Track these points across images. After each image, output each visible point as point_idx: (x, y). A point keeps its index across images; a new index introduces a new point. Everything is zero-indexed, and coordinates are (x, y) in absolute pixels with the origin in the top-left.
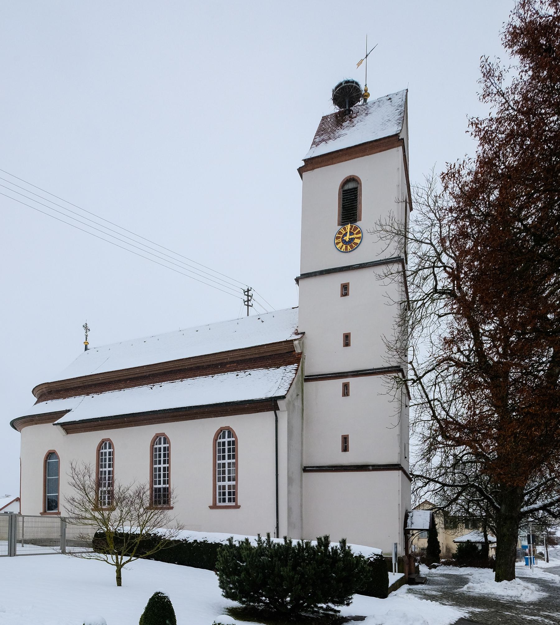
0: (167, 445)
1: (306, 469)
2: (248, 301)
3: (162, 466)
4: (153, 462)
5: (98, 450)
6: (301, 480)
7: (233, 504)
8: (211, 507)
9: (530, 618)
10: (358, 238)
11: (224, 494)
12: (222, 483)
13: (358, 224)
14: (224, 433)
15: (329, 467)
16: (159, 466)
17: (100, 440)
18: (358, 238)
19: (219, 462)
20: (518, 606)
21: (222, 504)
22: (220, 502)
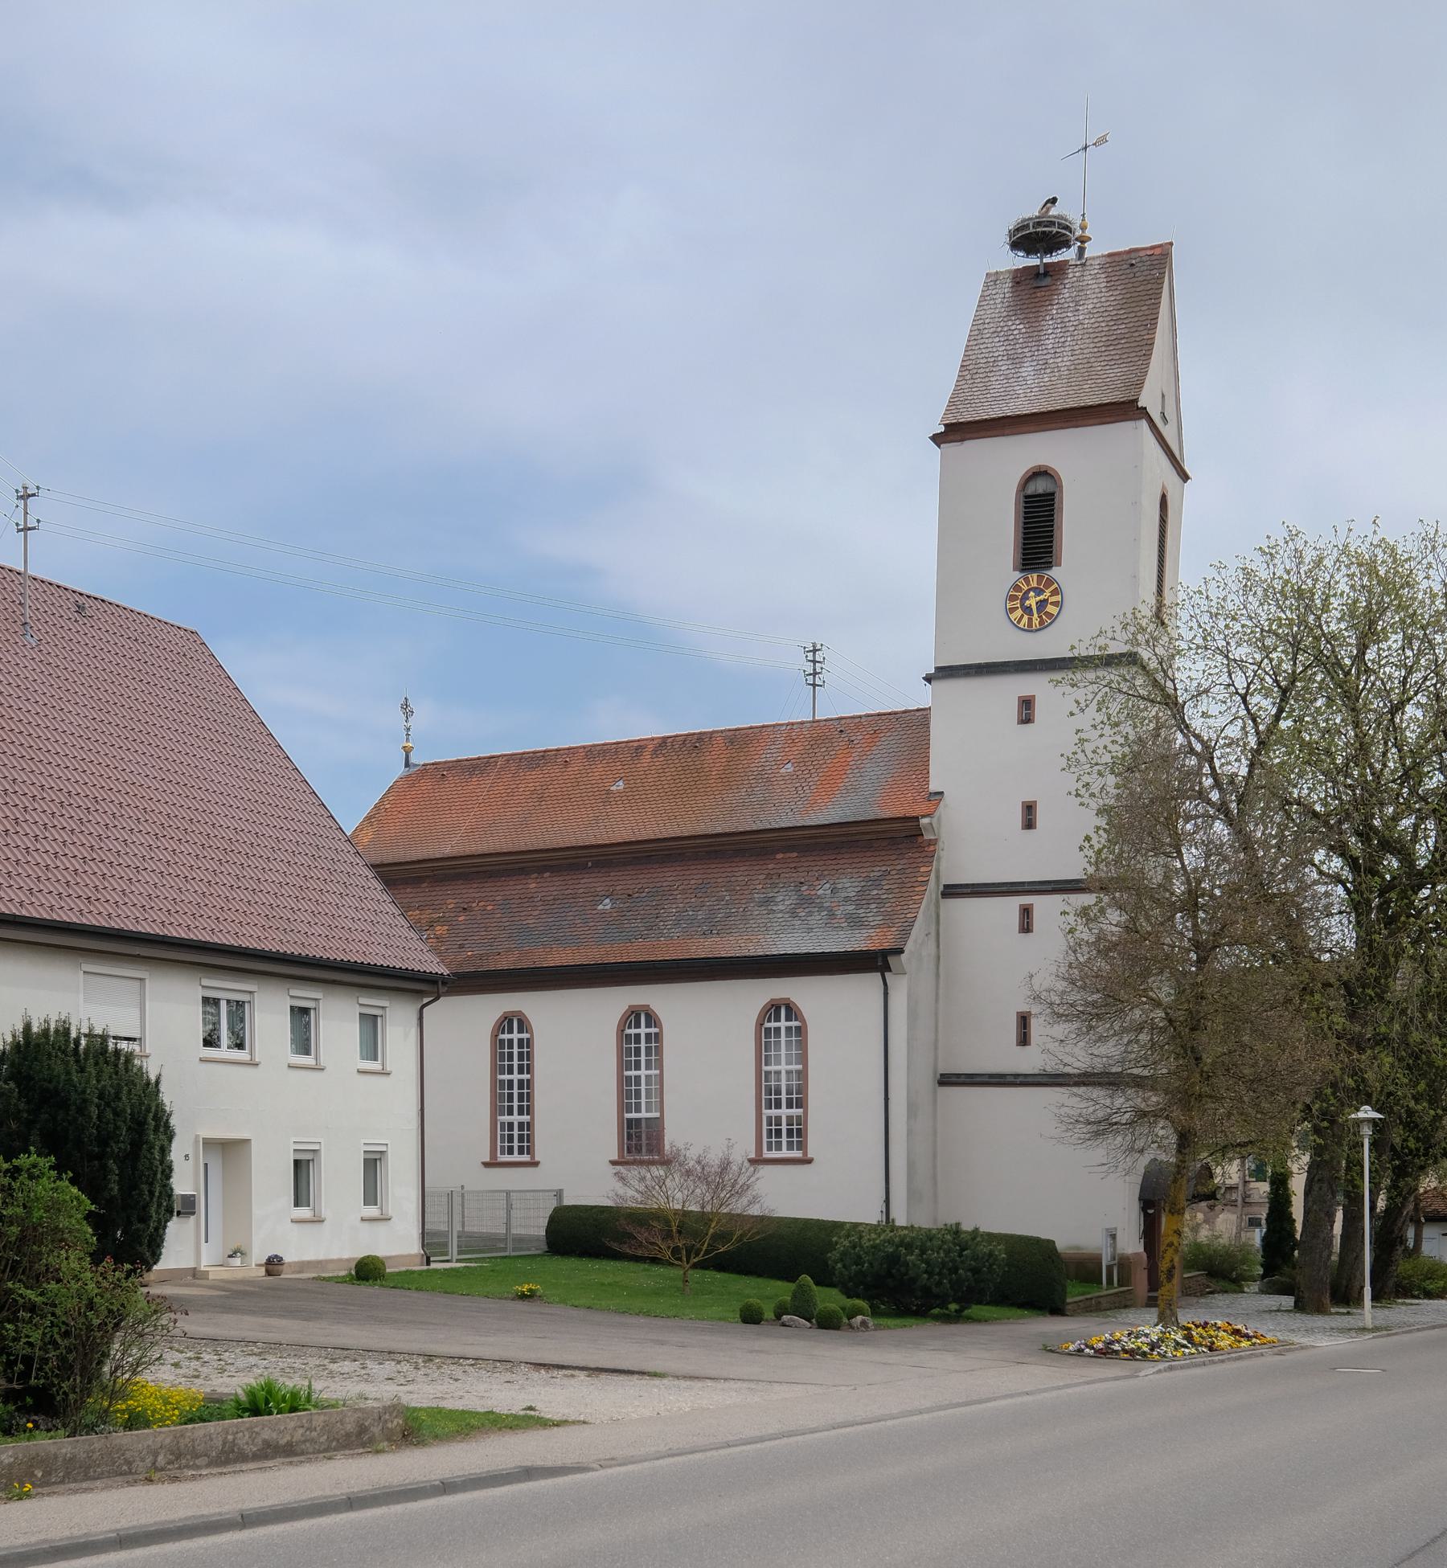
0: (525, 1036)
1: (947, 1080)
2: (815, 674)
3: (516, 1077)
4: (496, 1069)
5: (495, 1036)
6: (935, 1101)
7: (525, 1158)
8: (486, 1165)
10: (1055, 604)
11: (511, 1138)
12: (774, 1112)
13: (1054, 572)
14: (511, 1022)
15: (991, 1076)
16: (510, 1077)
17: (498, 1015)
18: (1055, 604)
19: (768, 1068)
21: (507, 1158)
22: (502, 1153)
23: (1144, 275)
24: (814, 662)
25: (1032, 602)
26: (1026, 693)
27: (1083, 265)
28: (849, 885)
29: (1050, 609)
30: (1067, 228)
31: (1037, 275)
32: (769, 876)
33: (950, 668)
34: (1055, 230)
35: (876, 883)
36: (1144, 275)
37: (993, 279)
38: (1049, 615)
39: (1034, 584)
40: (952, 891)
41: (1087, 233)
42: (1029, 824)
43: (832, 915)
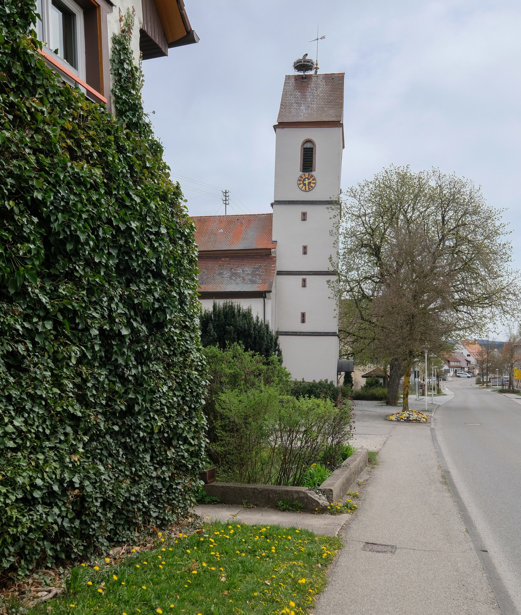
2: (226, 200)
9: (426, 356)
13: (313, 173)
15: (293, 332)
18: (314, 183)
20: (297, 477)
23: (336, 82)
24: (226, 196)
25: (307, 182)
26: (304, 211)
27: (317, 76)
28: (248, 270)
29: (312, 185)
30: (312, 63)
31: (303, 78)
32: (220, 265)
33: (280, 201)
34: (310, 64)
35: (258, 269)
36: (336, 82)
37: (288, 77)
38: (312, 187)
39: (307, 177)
40: (280, 273)
41: (318, 66)
42: (305, 253)
43: (244, 279)
